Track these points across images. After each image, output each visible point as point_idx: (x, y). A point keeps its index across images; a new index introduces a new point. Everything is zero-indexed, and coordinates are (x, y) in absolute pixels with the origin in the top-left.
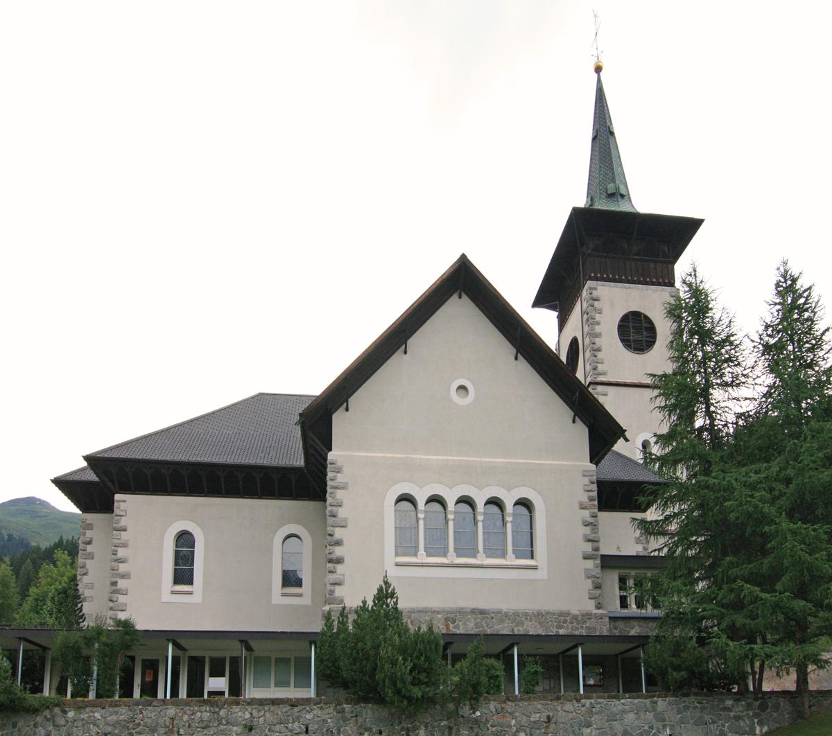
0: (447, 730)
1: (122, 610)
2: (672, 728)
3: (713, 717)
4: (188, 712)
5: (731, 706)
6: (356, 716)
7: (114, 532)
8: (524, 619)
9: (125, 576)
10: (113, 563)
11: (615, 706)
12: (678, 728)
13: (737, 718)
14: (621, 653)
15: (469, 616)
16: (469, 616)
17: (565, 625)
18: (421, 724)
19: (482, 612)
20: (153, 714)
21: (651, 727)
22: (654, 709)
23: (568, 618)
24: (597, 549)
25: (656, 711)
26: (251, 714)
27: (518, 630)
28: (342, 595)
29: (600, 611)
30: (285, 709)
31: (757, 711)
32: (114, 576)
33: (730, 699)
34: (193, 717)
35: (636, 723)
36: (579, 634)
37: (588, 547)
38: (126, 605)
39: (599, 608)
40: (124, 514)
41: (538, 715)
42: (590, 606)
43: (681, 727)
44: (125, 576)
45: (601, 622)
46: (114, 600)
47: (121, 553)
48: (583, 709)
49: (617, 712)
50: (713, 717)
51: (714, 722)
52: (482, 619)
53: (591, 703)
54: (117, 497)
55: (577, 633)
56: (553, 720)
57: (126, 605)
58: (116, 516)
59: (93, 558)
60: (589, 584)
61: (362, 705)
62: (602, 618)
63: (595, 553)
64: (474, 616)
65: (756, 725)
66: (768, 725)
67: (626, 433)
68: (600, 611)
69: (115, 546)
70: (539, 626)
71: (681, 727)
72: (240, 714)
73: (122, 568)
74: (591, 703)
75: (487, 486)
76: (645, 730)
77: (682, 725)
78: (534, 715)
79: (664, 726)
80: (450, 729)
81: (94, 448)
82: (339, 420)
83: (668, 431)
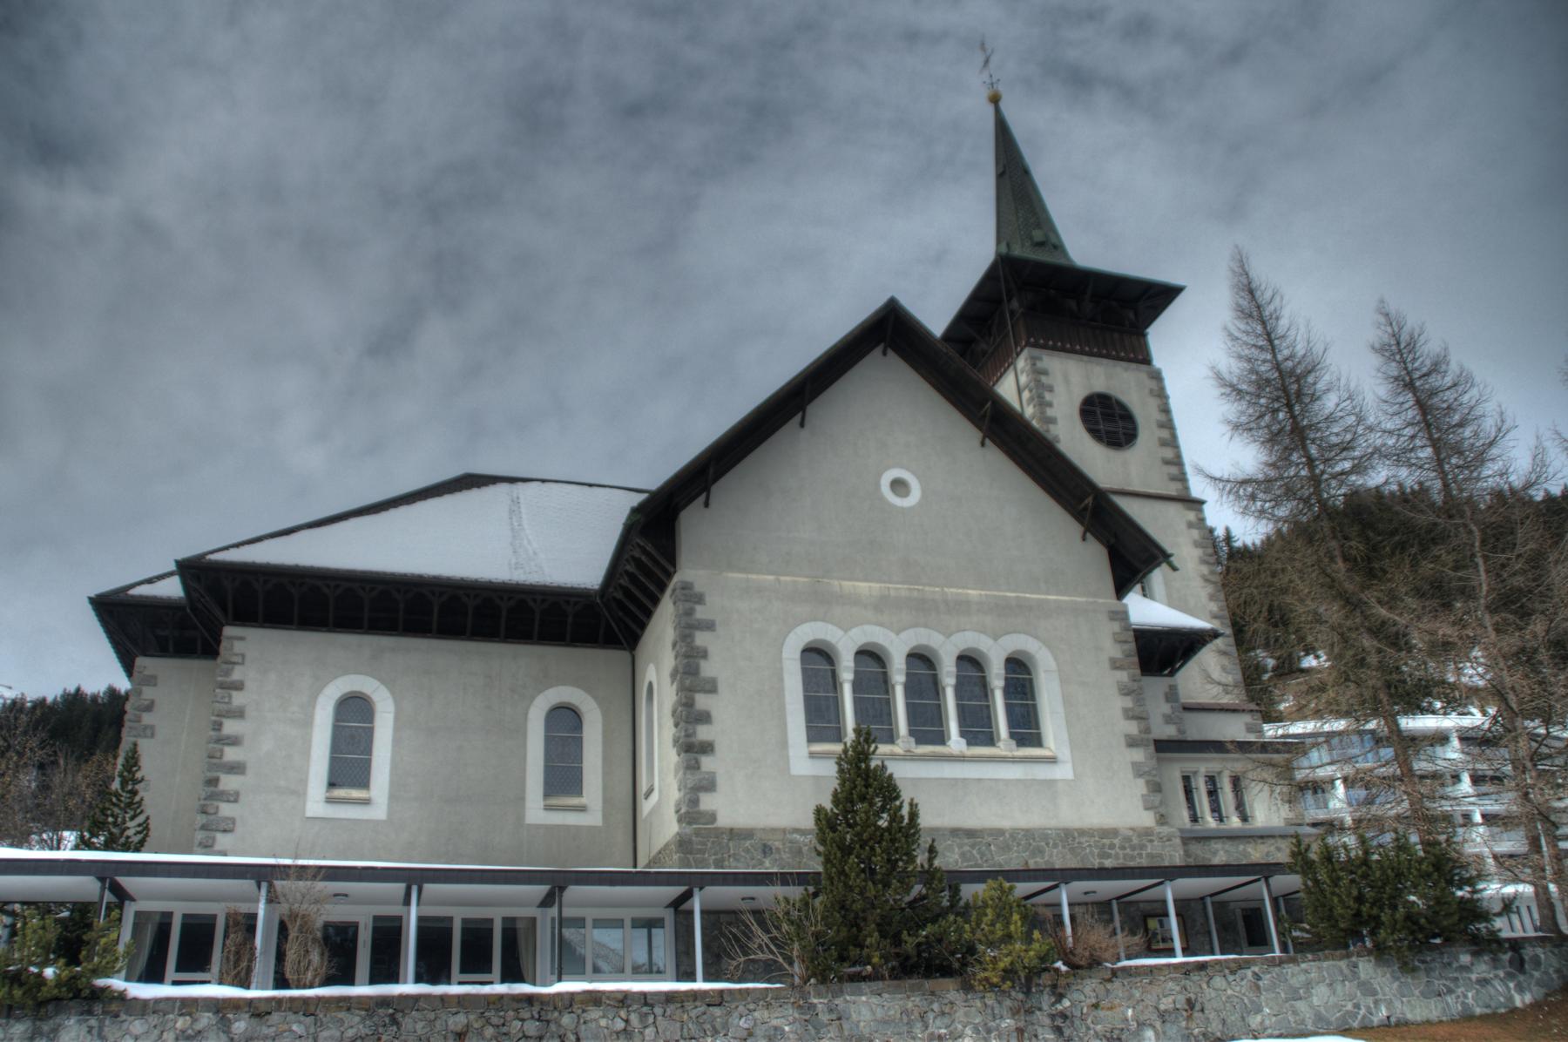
0: (1015, 1034)
1: (225, 831)
2: (1389, 1004)
3: (1448, 983)
4: (495, 1021)
5: (1468, 964)
6: (839, 1019)
7: (218, 691)
8: (1043, 844)
9: (237, 768)
10: (211, 745)
11: (1293, 975)
12: (1398, 1004)
13: (1484, 982)
14: (1212, 895)
15: (949, 842)
16: (949, 842)
17: (1113, 852)
18: (965, 1027)
19: (971, 833)
20: (420, 1025)
21: (1357, 1006)
22: (1355, 974)
23: (1116, 841)
24: (1147, 730)
25: (1359, 978)
26: (627, 1021)
27: (1036, 862)
28: (714, 808)
29: (1165, 830)
30: (695, 1011)
31: (1509, 969)
32: (211, 767)
33: (1467, 952)
34: (504, 1030)
35: (1333, 1000)
36: (1137, 865)
37: (1133, 728)
38: (233, 821)
39: (1162, 824)
40: (240, 661)
41: (1170, 999)
42: (1147, 819)
43: (1402, 1002)
44: (237, 768)
45: (1170, 846)
46: (212, 811)
47: (230, 727)
48: (1244, 983)
49: (1298, 986)
50: (1448, 983)
51: (1450, 991)
52: (973, 846)
53: (1255, 974)
54: (229, 631)
55: (1132, 864)
56: (1198, 1007)
57: (233, 821)
58: (226, 663)
59: (153, 735)
60: (1140, 787)
61: (848, 998)
62: (1169, 840)
63: (1146, 736)
64: (958, 841)
65: (1513, 992)
66: (1531, 991)
67: (1172, 559)
68: (1165, 830)
69: (218, 716)
70: (1069, 856)
71: (1402, 1002)
72: (603, 1022)
73: (231, 754)
74: (1255, 974)
75: (959, 631)
76: (1347, 1011)
77: (1404, 999)
78: (1164, 1000)
79: (1376, 1003)
80: (1020, 1031)
81: (180, 557)
82: (694, 525)
83: (1249, 542)
